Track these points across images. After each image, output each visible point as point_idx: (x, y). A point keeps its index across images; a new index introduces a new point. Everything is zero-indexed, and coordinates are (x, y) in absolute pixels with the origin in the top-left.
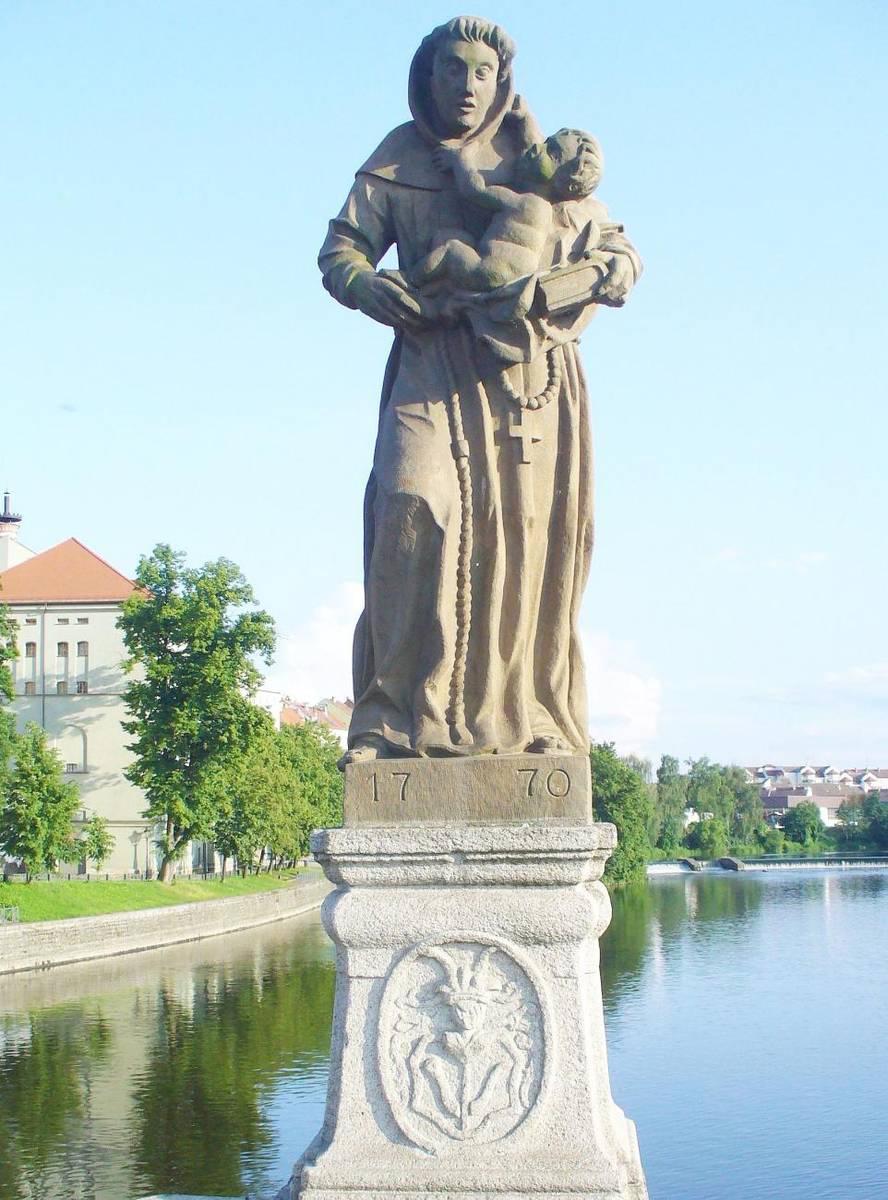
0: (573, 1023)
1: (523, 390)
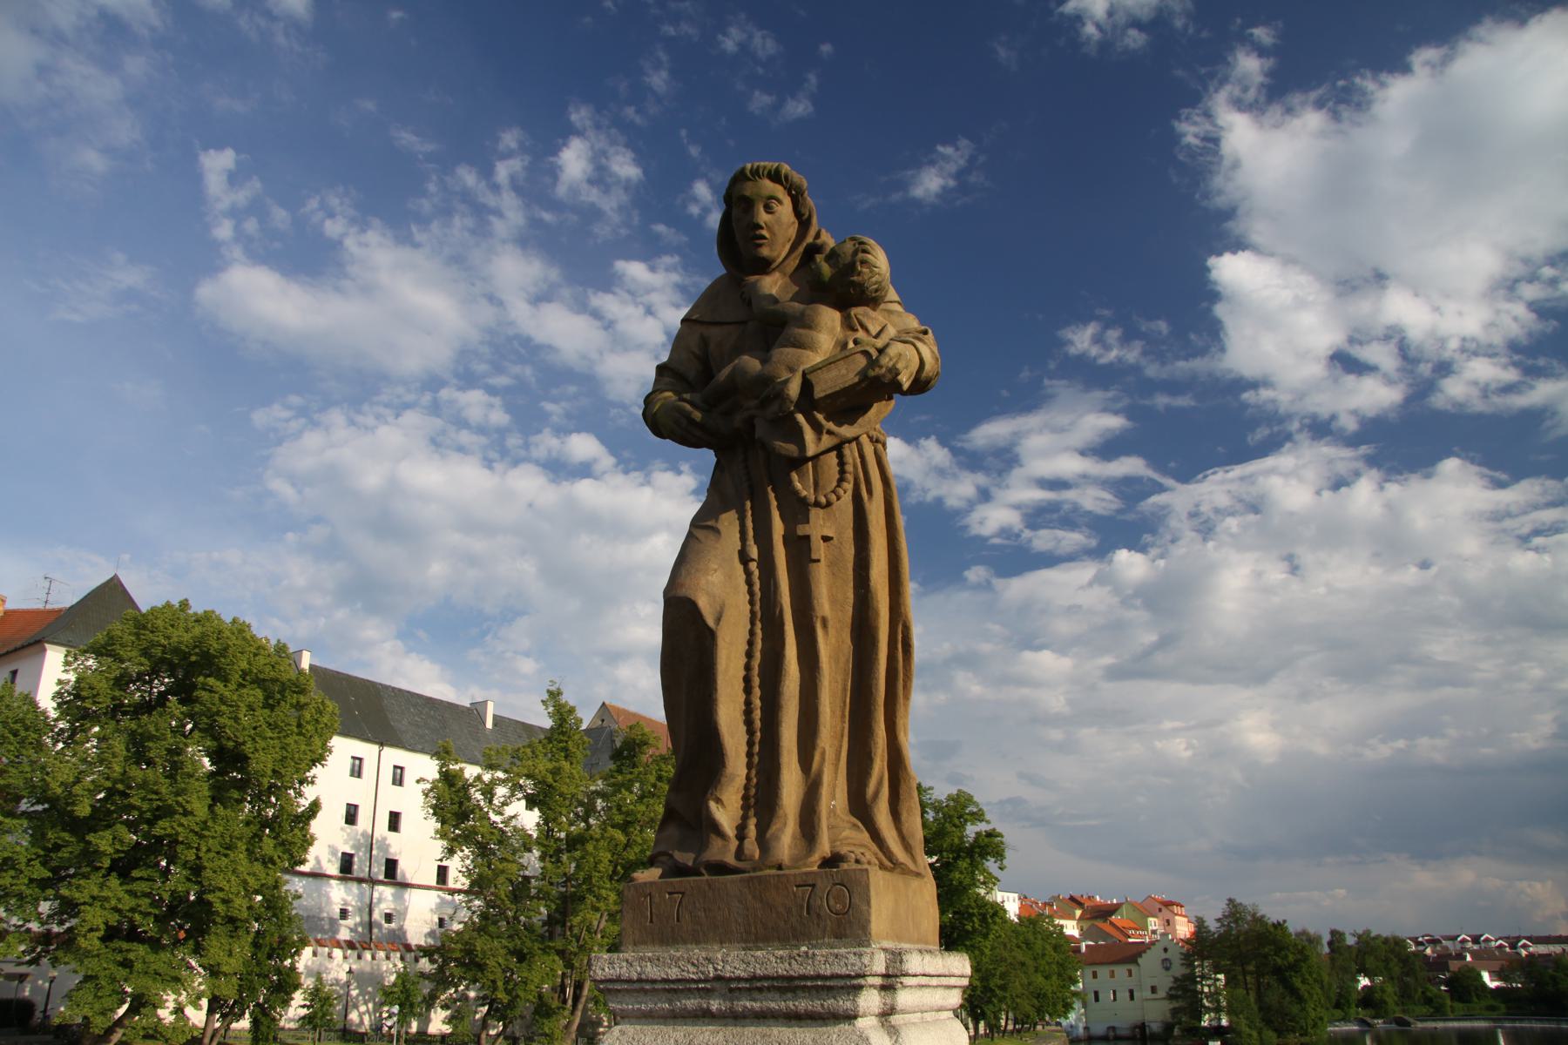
1: (812, 491)
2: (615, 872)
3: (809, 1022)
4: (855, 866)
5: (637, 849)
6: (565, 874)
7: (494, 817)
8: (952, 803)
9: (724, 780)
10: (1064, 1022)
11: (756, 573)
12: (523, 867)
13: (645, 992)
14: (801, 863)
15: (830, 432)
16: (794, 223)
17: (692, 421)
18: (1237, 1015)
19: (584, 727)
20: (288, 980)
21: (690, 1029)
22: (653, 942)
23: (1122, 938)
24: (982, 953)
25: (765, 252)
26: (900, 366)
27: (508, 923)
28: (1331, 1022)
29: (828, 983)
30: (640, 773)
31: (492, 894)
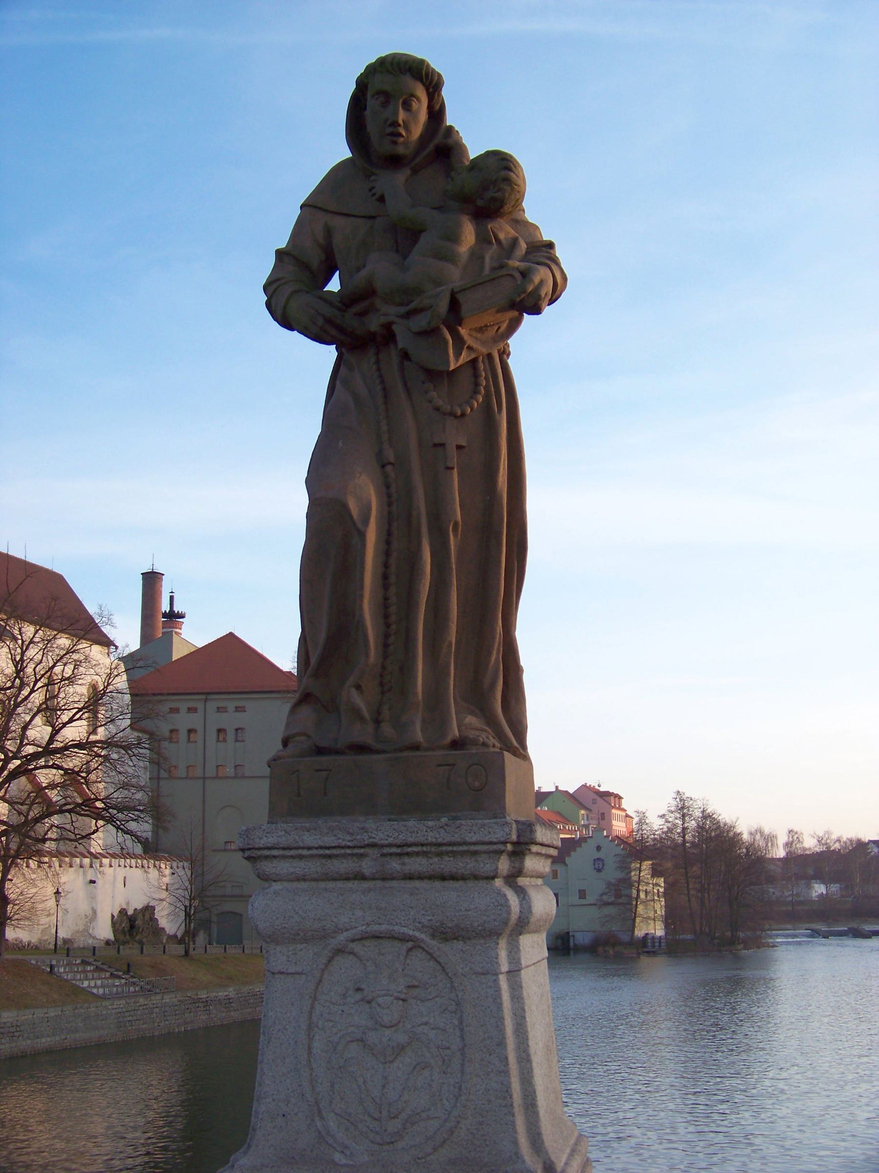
15: (470, 348)
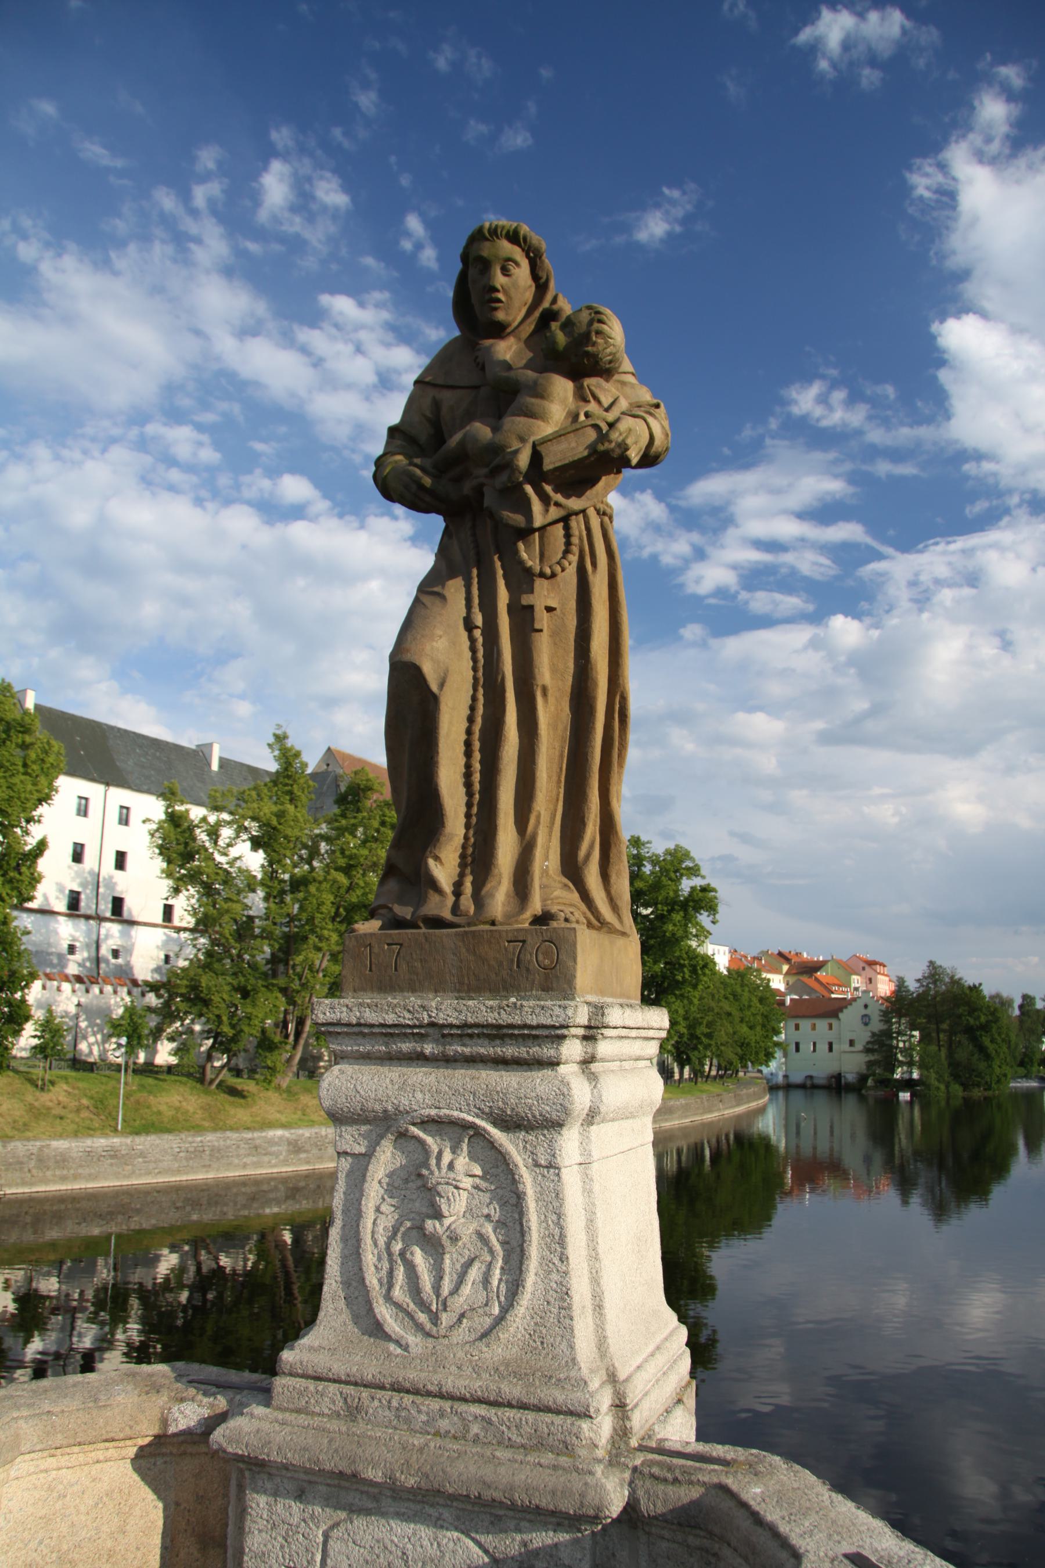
0: (554, 1217)
2: (337, 914)
3: (515, 1066)
4: (564, 925)
5: (359, 892)
6: (288, 915)
7: (219, 858)
8: (669, 858)
9: (442, 839)
10: (765, 1070)
11: (480, 640)
12: (247, 907)
13: (364, 1035)
14: (513, 920)
15: (557, 504)
16: (531, 286)
17: (421, 487)
18: (927, 1070)
19: (309, 771)
20: (18, 1011)
21: (405, 1070)
22: (372, 990)
23: (826, 994)
24: (691, 1003)
25: (500, 316)
26: (629, 441)
27: (232, 960)
28: (1014, 1078)
29: (534, 1032)
30: (363, 818)
31: (217, 932)
